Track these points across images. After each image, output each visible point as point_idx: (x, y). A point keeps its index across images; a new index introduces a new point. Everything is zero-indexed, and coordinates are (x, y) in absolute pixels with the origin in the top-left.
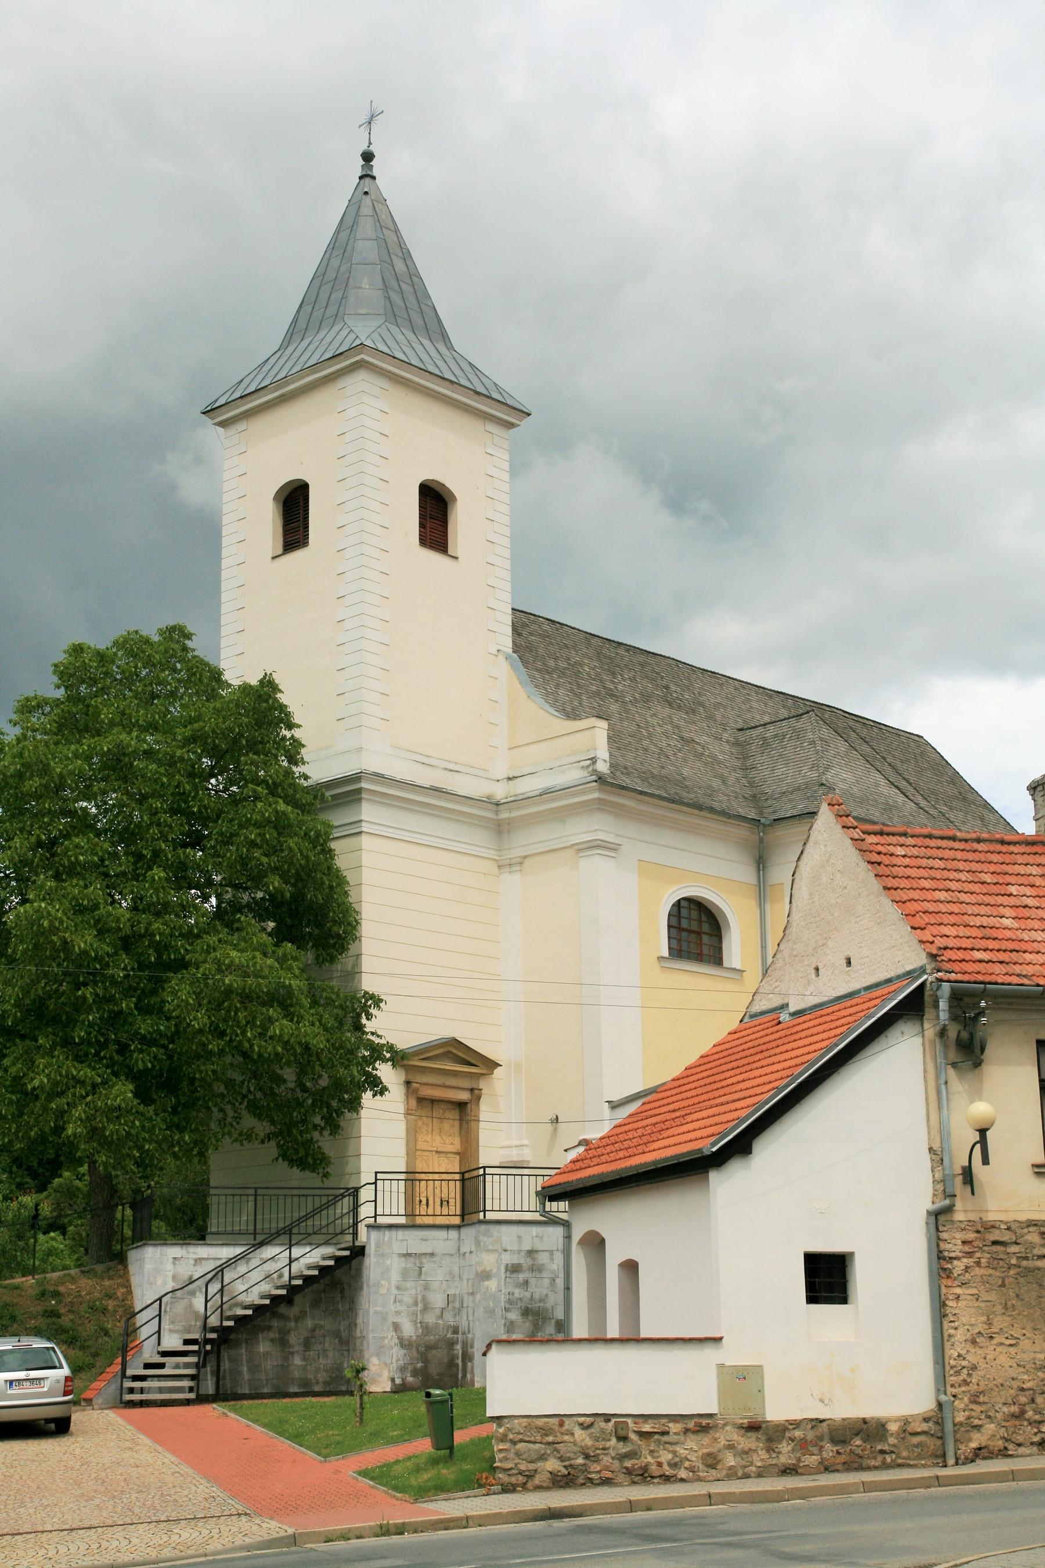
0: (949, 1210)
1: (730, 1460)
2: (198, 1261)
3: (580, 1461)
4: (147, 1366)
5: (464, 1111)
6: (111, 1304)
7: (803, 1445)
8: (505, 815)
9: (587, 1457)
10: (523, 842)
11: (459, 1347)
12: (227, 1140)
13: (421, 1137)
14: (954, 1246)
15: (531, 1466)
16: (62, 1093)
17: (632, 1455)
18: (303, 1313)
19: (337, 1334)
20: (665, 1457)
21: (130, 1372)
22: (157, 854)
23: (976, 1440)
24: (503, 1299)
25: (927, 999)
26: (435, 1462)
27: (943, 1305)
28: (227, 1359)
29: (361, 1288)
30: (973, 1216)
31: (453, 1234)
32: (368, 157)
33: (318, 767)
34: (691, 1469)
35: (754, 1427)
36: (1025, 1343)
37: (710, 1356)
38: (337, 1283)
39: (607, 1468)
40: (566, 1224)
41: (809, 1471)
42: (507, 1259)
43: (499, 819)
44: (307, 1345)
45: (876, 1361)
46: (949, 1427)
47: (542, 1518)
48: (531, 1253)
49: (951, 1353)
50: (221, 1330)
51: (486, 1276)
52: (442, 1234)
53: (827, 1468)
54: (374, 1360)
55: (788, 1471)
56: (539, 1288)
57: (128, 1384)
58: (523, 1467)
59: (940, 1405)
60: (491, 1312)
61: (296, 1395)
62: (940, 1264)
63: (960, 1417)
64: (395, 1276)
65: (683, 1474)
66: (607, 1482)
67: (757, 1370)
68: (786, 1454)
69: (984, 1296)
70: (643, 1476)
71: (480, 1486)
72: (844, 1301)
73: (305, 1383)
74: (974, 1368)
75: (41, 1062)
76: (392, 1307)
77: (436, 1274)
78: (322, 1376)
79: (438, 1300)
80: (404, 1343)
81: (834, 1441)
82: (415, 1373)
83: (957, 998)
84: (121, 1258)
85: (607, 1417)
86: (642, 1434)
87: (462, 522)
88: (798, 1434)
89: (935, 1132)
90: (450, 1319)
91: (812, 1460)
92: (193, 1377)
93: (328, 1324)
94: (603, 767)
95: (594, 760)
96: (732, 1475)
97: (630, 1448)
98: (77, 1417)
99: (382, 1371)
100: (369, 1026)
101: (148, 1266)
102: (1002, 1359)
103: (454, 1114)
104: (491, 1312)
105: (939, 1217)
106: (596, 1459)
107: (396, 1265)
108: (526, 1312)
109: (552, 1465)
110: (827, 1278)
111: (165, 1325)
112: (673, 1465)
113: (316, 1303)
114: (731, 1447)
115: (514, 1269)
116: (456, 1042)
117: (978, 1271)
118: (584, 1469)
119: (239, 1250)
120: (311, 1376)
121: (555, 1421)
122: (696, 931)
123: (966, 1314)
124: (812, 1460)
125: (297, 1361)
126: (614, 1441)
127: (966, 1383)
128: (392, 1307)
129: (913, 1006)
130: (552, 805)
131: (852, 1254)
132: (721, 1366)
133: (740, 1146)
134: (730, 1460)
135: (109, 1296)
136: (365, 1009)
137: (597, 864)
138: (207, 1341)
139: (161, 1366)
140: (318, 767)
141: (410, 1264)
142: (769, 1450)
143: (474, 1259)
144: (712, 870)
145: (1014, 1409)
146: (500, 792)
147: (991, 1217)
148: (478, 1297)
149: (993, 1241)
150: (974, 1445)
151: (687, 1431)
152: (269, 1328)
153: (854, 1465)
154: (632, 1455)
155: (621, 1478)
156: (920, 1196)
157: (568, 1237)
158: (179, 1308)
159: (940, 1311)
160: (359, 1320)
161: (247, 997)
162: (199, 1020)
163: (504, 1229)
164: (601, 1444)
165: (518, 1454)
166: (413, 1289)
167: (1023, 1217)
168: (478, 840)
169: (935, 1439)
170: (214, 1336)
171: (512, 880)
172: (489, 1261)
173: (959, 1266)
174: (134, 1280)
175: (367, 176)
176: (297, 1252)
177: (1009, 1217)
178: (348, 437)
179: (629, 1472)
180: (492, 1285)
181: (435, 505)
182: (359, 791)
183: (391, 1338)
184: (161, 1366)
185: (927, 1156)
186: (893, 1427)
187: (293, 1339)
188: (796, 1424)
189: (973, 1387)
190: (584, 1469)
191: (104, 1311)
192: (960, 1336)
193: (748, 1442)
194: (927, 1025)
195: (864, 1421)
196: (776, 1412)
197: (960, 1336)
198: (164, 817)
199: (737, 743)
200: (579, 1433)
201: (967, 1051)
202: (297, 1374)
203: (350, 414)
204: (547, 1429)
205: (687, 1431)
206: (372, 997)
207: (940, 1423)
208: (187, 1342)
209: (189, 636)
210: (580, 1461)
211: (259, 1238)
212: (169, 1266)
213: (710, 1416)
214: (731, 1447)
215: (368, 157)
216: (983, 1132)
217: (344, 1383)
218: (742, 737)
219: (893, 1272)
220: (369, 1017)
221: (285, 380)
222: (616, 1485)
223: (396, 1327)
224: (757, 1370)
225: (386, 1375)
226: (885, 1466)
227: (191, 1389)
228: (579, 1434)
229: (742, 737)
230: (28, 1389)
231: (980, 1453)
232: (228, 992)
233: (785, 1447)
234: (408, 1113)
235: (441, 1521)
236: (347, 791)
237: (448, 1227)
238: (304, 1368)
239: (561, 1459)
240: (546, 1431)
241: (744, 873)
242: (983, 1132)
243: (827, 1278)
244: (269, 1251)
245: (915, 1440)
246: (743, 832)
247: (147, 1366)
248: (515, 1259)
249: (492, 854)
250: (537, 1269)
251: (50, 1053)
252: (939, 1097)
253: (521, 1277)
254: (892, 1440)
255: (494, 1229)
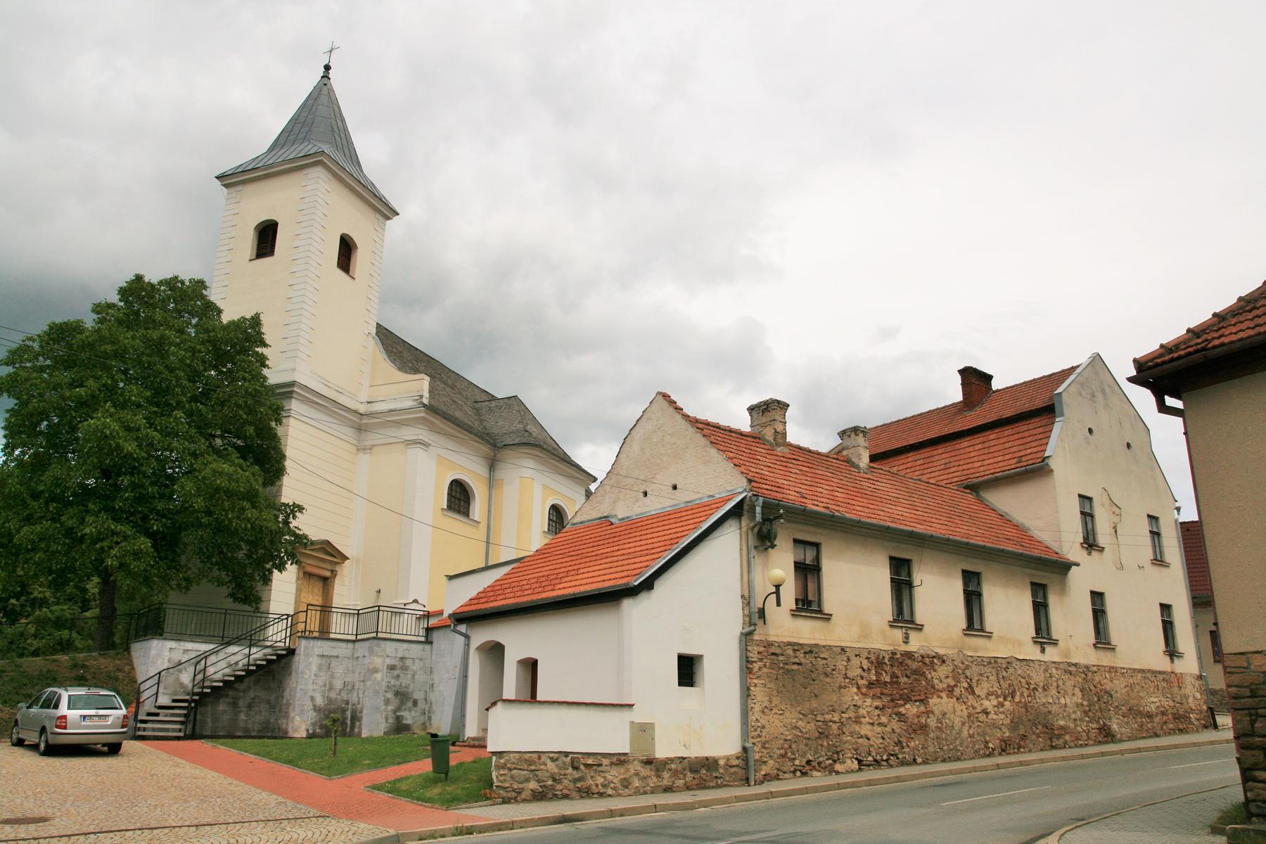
0: (750, 633)
1: (637, 783)
2: (186, 651)
3: (550, 782)
4: (149, 714)
5: (326, 582)
6: (120, 675)
7: (675, 773)
8: (365, 421)
9: (554, 780)
10: (371, 438)
11: (349, 714)
12: (205, 580)
13: (303, 594)
14: (754, 656)
15: (521, 786)
16: (102, 540)
17: (581, 779)
18: (249, 687)
19: (268, 702)
20: (600, 780)
21: (140, 718)
22: (179, 403)
23: (764, 770)
24: (384, 685)
25: (746, 507)
26: (436, 782)
27: (748, 689)
28: (203, 715)
29: (290, 674)
30: (763, 638)
31: (350, 645)
32: (327, 68)
33: (273, 376)
34: (614, 789)
35: (649, 762)
36: (787, 714)
37: (625, 717)
38: (276, 668)
39: (566, 788)
40: (467, 637)
41: (679, 790)
42: (388, 661)
43: (362, 424)
44: (250, 707)
45: (707, 724)
46: (752, 763)
47: (555, 823)
48: (402, 659)
49: (752, 718)
50: (202, 695)
51: (376, 671)
52: (344, 645)
53: (688, 788)
54: (298, 718)
55: (668, 789)
56: (405, 680)
57: (139, 725)
58: (515, 786)
59: (745, 749)
60: (376, 693)
61: (240, 737)
62: (747, 667)
63: (757, 757)
64: (314, 668)
65: (610, 792)
66: (566, 797)
67: (652, 726)
68: (667, 779)
69: (769, 685)
70: (586, 793)
71: (487, 799)
72: (680, 684)
73: (246, 730)
74: (763, 727)
75: (89, 519)
76: (311, 687)
77: (338, 669)
78: (257, 727)
79: (338, 684)
80: (316, 709)
81: (692, 771)
82: (321, 727)
83: (766, 506)
84: (128, 649)
85: (566, 754)
86: (587, 766)
87: (360, 259)
88: (673, 766)
89: (746, 586)
90: (344, 696)
91: (680, 783)
92: (182, 723)
93: (263, 695)
94: (426, 401)
95: (421, 397)
96: (638, 792)
97: (575, 775)
98: (127, 745)
99: (300, 723)
100: (293, 523)
101: (153, 652)
102: (777, 723)
103: (320, 585)
104: (376, 693)
105: (747, 637)
106: (560, 781)
107: (315, 662)
108: (397, 694)
109: (533, 785)
110: (688, 669)
111: (161, 690)
112: (604, 786)
113: (257, 682)
114: (637, 774)
115: (392, 668)
116: (328, 543)
117: (765, 670)
118: (553, 788)
119: (212, 646)
120: (250, 726)
121: (535, 755)
122: (459, 498)
123: (760, 695)
124: (680, 783)
125: (243, 717)
126: (570, 770)
127: (759, 736)
128: (311, 687)
129: (737, 512)
130: (394, 419)
131: (701, 657)
132: (632, 723)
133: (648, 585)
134: (636, 783)
135: (119, 670)
136: (293, 512)
137: (418, 452)
138: (194, 701)
139: (157, 715)
140: (273, 376)
141: (324, 661)
142: (658, 776)
143: (367, 661)
144: (470, 469)
145: (782, 751)
146: (363, 409)
147: (771, 639)
148: (369, 683)
149: (773, 652)
150: (763, 773)
151: (612, 764)
152: (227, 696)
153: (702, 786)
154: (581, 779)
155: (574, 794)
156: (735, 624)
157: (468, 645)
158: (171, 679)
159: (746, 693)
160: (287, 694)
161: (230, 494)
162: (199, 503)
163: (388, 643)
164: (563, 772)
165: (512, 777)
166: (324, 677)
167: (786, 640)
168: (348, 432)
169: (743, 769)
170: (196, 698)
171: (364, 458)
172: (378, 661)
173: (756, 666)
174: (136, 662)
175: (326, 76)
176: (254, 650)
177: (779, 639)
178: (306, 200)
179: (579, 790)
180: (378, 676)
181: (347, 249)
182: (292, 392)
183: (308, 705)
184: (157, 715)
185: (740, 601)
186: (722, 762)
187: (241, 703)
188: (671, 760)
189: (763, 739)
190: (553, 788)
191: (116, 679)
192: (757, 708)
193: (645, 771)
194: (744, 523)
195: (707, 759)
196: (661, 753)
197: (757, 708)
198: (184, 382)
199: (474, 408)
200: (550, 764)
201: (764, 539)
202: (242, 725)
203: (309, 188)
204: (531, 760)
205: (612, 764)
206: (298, 506)
207: (746, 760)
208: (174, 701)
209: (205, 288)
210: (550, 782)
211: (226, 640)
212: (167, 653)
213: (625, 754)
214: (637, 774)
215: (327, 68)
216: (778, 587)
217: (272, 732)
218: (477, 406)
219: (722, 669)
220: (294, 517)
221: (272, 166)
222: (572, 799)
223: (312, 699)
224: (652, 726)
225: (304, 727)
226: (719, 786)
227: (180, 730)
228: (551, 765)
229: (477, 406)
230: (97, 722)
231: (767, 778)
232: (218, 489)
233: (666, 775)
234: (298, 579)
235: (496, 824)
236: (288, 390)
237: (348, 641)
238: (246, 721)
239: (538, 781)
240: (530, 762)
241: (482, 470)
242: (778, 587)
243: (688, 669)
244: (233, 649)
245: (733, 770)
246: (485, 449)
247: (149, 714)
248: (394, 662)
249: (355, 442)
250: (405, 668)
251: (97, 514)
252: (748, 567)
253: (396, 672)
254: (721, 770)
255: (382, 643)
